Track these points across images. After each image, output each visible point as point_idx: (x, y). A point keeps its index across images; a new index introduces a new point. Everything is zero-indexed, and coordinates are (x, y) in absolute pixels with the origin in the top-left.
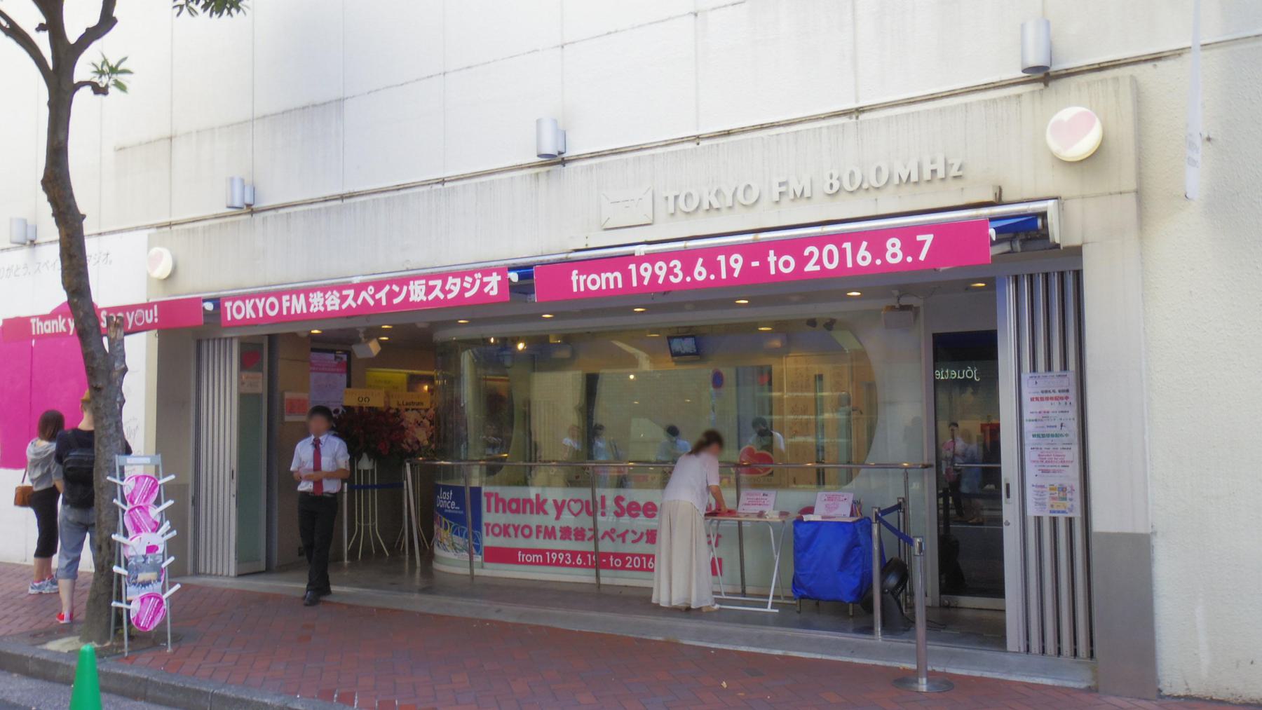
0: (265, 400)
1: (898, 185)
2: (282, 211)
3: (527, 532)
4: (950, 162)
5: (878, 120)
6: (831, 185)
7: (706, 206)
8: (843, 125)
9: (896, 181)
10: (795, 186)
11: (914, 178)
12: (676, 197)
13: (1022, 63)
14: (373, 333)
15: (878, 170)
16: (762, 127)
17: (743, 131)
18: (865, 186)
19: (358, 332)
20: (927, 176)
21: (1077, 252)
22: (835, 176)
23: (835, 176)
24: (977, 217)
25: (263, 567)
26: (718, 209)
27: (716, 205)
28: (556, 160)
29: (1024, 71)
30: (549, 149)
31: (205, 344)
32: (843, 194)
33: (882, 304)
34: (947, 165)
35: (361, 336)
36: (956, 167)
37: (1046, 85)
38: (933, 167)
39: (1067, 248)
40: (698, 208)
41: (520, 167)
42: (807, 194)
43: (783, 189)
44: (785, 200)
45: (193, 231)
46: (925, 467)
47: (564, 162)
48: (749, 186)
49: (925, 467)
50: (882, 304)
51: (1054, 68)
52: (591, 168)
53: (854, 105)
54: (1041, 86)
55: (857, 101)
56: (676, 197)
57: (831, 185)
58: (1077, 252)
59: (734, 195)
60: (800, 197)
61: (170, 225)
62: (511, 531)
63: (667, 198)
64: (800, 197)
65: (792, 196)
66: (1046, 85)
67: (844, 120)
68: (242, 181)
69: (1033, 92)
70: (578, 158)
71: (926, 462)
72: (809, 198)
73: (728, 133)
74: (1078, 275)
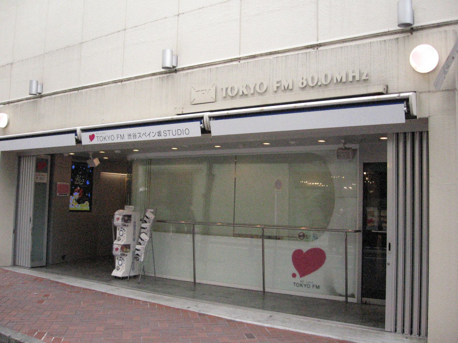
0: (48, 186)
1: (336, 84)
2: (53, 96)
3: (309, 286)
4: (362, 72)
5: (326, 50)
6: (302, 83)
7: (241, 93)
8: (309, 52)
9: (335, 81)
10: (285, 83)
11: (344, 80)
12: (227, 89)
13: (398, 21)
14: (96, 155)
15: (326, 76)
16: (271, 54)
17: (261, 55)
18: (319, 84)
19: (89, 155)
20: (350, 79)
21: (426, 121)
22: (304, 79)
23: (304, 79)
24: (373, 99)
25: (44, 264)
26: (246, 95)
27: (246, 93)
28: (172, 70)
29: (399, 25)
30: (168, 65)
31: (22, 159)
32: (308, 88)
33: (335, 147)
34: (361, 74)
35: (91, 156)
36: (365, 75)
37: (412, 34)
38: (354, 74)
39: (420, 119)
40: (237, 94)
41: (154, 74)
42: (290, 87)
43: (279, 85)
44: (280, 91)
45: (17, 106)
46: (356, 231)
47: (176, 71)
48: (262, 83)
49: (356, 231)
50: (335, 147)
51: (415, 25)
52: (187, 74)
53: (315, 42)
54: (409, 34)
55: (318, 40)
56: (227, 89)
57: (302, 83)
58: (426, 121)
59: (254, 88)
60: (287, 89)
61: (9, 103)
62: (303, 285)
63: (222, 89)
64: (287, 89)
65: (283, 88)
66: (412, 34)
67: (311, 50)
68: (37, 82)
69: (404, 37)
70: (183, 69)
71: (357, 229)
72: (291, 90)
73: (254, 57)
74: (428, 132)
